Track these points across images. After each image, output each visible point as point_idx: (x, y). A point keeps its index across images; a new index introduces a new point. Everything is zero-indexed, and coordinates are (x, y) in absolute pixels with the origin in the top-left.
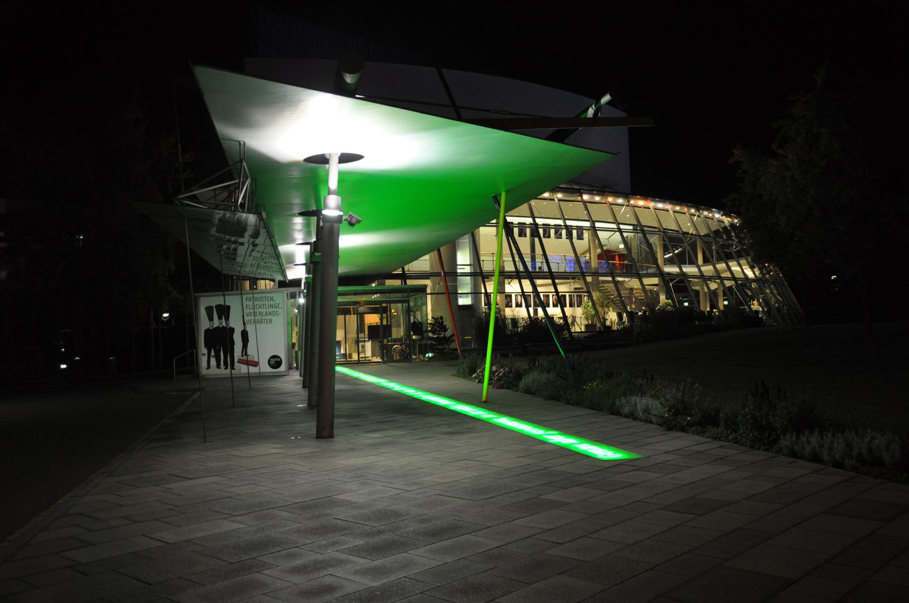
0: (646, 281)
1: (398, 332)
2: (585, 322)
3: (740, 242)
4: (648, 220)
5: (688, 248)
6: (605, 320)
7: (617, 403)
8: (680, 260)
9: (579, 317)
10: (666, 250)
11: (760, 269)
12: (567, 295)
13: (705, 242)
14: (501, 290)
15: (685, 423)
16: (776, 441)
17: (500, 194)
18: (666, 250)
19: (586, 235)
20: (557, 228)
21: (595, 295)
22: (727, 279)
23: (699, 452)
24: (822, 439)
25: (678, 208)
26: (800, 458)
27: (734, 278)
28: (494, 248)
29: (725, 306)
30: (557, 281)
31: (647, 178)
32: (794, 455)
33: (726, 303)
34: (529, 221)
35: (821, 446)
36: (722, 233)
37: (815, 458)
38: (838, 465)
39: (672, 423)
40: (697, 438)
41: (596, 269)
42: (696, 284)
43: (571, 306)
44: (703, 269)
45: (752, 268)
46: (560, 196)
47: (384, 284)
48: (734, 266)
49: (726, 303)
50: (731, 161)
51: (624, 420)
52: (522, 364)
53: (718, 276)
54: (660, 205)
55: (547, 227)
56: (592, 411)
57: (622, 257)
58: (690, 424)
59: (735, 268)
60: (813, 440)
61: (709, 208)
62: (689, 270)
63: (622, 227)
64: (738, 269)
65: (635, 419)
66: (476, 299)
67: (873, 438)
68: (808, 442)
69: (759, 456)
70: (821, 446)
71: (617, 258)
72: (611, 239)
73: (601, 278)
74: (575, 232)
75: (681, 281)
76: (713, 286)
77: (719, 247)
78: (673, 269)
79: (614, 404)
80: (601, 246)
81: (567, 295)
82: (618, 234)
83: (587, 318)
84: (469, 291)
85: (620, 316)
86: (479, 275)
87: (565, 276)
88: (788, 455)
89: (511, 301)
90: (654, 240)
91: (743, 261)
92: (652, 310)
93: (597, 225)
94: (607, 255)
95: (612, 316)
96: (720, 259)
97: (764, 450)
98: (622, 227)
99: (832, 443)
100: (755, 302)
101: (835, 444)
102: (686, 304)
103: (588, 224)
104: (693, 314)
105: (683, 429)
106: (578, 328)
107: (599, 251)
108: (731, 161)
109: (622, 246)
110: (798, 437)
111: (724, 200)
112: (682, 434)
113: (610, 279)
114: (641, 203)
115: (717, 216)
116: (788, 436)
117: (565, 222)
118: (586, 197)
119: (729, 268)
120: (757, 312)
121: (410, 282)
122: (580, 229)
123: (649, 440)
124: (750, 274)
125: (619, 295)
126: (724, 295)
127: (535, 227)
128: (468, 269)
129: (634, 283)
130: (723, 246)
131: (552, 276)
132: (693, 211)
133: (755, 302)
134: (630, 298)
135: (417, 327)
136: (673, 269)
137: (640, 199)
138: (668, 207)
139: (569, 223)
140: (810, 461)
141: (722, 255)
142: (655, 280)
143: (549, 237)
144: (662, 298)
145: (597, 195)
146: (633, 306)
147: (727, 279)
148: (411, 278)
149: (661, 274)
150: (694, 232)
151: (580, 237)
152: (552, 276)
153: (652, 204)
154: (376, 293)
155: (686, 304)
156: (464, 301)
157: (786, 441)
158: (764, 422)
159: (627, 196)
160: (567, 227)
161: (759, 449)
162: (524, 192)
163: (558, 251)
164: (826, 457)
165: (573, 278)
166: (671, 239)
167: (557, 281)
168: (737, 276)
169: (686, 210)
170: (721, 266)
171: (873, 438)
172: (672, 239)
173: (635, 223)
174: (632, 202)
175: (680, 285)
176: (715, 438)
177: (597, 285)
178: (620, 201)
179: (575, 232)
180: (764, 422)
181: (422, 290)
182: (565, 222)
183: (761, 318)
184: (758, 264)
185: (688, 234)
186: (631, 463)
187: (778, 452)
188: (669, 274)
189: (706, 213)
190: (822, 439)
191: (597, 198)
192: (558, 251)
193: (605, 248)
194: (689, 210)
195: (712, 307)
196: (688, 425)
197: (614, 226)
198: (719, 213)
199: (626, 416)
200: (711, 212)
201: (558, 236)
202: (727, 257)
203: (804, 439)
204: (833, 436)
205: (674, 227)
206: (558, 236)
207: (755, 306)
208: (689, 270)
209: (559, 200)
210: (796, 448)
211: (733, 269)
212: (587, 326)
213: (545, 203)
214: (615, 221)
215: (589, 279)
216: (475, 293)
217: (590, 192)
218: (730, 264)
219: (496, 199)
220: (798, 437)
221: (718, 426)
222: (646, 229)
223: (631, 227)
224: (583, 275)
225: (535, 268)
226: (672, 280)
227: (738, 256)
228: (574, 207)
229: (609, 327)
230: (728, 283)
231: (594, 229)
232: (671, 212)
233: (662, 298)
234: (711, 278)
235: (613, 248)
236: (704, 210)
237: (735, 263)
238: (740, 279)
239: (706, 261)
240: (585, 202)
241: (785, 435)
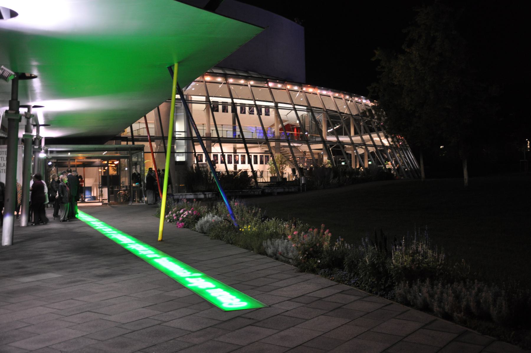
0: (313, 147)
1: (125, 180)
2: (270, 175)
3: (379, 119)
4: (315, 103)
5: (344, 126)
6: (283, 173)
7: (264, 244)
8: (338, 133)
9: (264, 172)
10: (328, 126)
11: (392, 138)
12: (259, 155)
13: (355, 120)
14: (207, 152)
15: (315, 266)
16: (391, 287)
17: (174, 65)
18: (328, 126)
19: (272, 112)
20: (250, 106)
21: (277, 155)
22: (370, 146)
23: (321, 299)
24: (432, 288)
25: (337, 95)
26: (412, 306)
27: (374, 145)
28: (205, 121)
29: (369, 165)
30: (248, 145)
31: (316, 75)
32: (406, 303)
33: (370, 163)
34: (229, 100)
35: (432, 296)
36: (365, 113)
37: (426, 308)
38: (447, 316)
39: (311, 261)
40: (325, 281)
41: (278, 137)
42: (349, 149)
43: (262, 163)
44: (353, 139)
45: (387, 137)
46: (252, 83)
47: (120, 144)
48: (375, 137)
49: (370, 163)
50: (373, 59)
51: (269, 260)
52: (203, 208)
53: (363, 144)
54: (324, 92)
55: (243, 106)
56: (245, 251)
57: (298, 129)
58: (320, 267)
59: (376, 139)
60: (425, 290)
61: (359, 95)
62: (344, 139)
63: (296, 107)
64: (378, 139)
65: (277, 259)
66: (189, 158)
67: (480, 290)
68: (420, 291)
69: (373, 303)
70: (432, 296)
71: (295, 130)
72: (288, 115)
73: (282, 144)
74: (263, 110)
75: (338, 147)
76: (361, 151)
77: (365, 123)
78: (333, 139)
79: (261, 245)
80: (281, 122)
81: (259, 155)
82: (293, 112)
83: (271, 172)
84: (184, 151)
85: (294, 171)
86: (192, 139)
87: (255, 142)
88: (401, 303)
89: (217, 159)
90: (320, 117)
91: (381, 134)
92: (316, 167)
93: (279, 105)
94: (287, 128)
95: (288, 171)
96: (366, 132)
97: (382, 296)
98: (296, 107)
99: (442, 293)
100: (389, 163)
101: (445, 295)
102: (343, 163)
103: (273, 104)
104: (348, 172)
105: (313, 271)
106: (267, 178)
107: (280, 126)
108: (373, 59)
109: (298, 122)
110: (411, 286)
111: (368, 88)
112: (312, 276)
113: (287, 144)
114: (311, 90)
115: (364, 101)
116: (402, 285)
117: (255, 102)
118: (271, 84)
119: (372, 139)
120: (390, 169)
121: (136, 143)
122: (267, 108)
123: (280, 284)
124: (385, 142)
125: (294, 157)
126: (369, 158)
127: (234, 105)
128: (183, 135)
129: (304, 147)
130: (368, 123)
131: (244, 141)
132: (347, 97)
133: (389, 163)
134: (303, 158)
135: (136, 178)
136: (333, 139)
137: (309, 87)
138: (330, 93)
139: (258, 103)
140: (422, 309)
141: (367, 129)
142: (321, 146)
143: (245, 113)
144: (325, 158)
145: (279, 83)
146: (306, 164)
147: (370, 146)
148: (138, 140)
149: (324, 142)
150: (348, 113)
151: (267, 114)
152: (244, 141)
153: (318, 91)
154: (105, 151)
155: (343, 163)
156: (180, 158)
157: (400, 290)
158: (381, 269)
159: (301, 84)
160: (256, 106)
161: (377, 294)
162: (194, 66)
163: (250, 123)
164: (436, 308)
165: (260, 143)
166: (331, 117)
167: (248, 145)
168: (377, 144)
169: (342, 96)
170: (366, 137)
171: (480, 290)
172: (334, 118)
173: (307, 105)
174: (304, 89)
175: (337, 150)
176: (339, 281)
177: (278, 148)
178: (296, 88)
179: (263, 110)
180: (381, 269)
181: (141, 149)
182: (255, 102)
183: (393, 175)
184: (391, 134)
185: (344, 113)
186: (248, 316)
187: (392, 299)
188: (330, 142)
189: (356, 99)
190: (432, 288)
191: (279, 86)
192: (250, 123)
193: (285, 124)
194: (344, 97)
195: (360, 166)
196: (318, 267)
197: (291, 106)
198: (366, 99)
199: (271, 256)
200: (360, 98)
201: (251, 112)
202: (371, 131)
203: (415, 287)
204: (443, 285)
205: (334, 109)
206: (251, 112)
207: (389, 165)
208: (344, 139)
209: (252, 86)
210: (409, 297)
211: (374, 139)
212: (271, 178)
213: (241, 87)
214: (292, 103)
215: (273, 144)
216: (189, 153)
217: (274, 80)
218: (373, 135)
219: (171, 69)
220: (411, 286)
221: (343, 269)
222: (313, 109)
223: (305, 108)
224: (266, 142)
225: (236, 136)
226: (331, 146)
227: (377, 130)
228: (262, 92)
229: (285, 179)
230: (371, 149)
231: (277, 108)
232: (332, 97)
233: (325, 158)
234: (359, 145)
235: (292, 123)
236: (355, 96)
237: (376, 135)
238: (379, 146)
239: (356, 133)
240: (270, 89)
241: (399, 282)
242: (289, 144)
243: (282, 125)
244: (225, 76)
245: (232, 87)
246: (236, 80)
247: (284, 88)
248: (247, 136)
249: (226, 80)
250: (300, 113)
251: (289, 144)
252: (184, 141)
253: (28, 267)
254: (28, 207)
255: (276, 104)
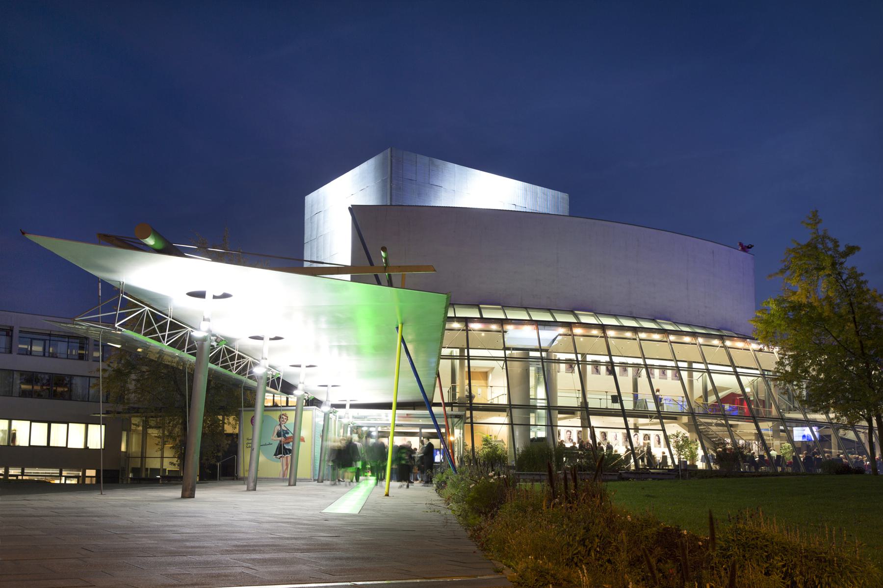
72: (726, 382)
82: (734, 377)
88: (71, 377)
98: (739, 370)
139: (648, 362)
197: (731, 369)
242: (727, 422)
243: (717, 396)
244: (722, 338)
245: (612, 342)
246: (588, 330)
247: (694, 342)
248: (592, 404)
249: (723, 343)
250: (745, 380)
251: (727, 422)
252: (503, 418)
253: (328, 559)
254: (232, 482)
255: (690, 363)
